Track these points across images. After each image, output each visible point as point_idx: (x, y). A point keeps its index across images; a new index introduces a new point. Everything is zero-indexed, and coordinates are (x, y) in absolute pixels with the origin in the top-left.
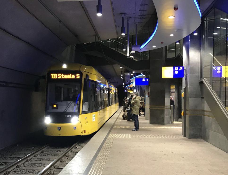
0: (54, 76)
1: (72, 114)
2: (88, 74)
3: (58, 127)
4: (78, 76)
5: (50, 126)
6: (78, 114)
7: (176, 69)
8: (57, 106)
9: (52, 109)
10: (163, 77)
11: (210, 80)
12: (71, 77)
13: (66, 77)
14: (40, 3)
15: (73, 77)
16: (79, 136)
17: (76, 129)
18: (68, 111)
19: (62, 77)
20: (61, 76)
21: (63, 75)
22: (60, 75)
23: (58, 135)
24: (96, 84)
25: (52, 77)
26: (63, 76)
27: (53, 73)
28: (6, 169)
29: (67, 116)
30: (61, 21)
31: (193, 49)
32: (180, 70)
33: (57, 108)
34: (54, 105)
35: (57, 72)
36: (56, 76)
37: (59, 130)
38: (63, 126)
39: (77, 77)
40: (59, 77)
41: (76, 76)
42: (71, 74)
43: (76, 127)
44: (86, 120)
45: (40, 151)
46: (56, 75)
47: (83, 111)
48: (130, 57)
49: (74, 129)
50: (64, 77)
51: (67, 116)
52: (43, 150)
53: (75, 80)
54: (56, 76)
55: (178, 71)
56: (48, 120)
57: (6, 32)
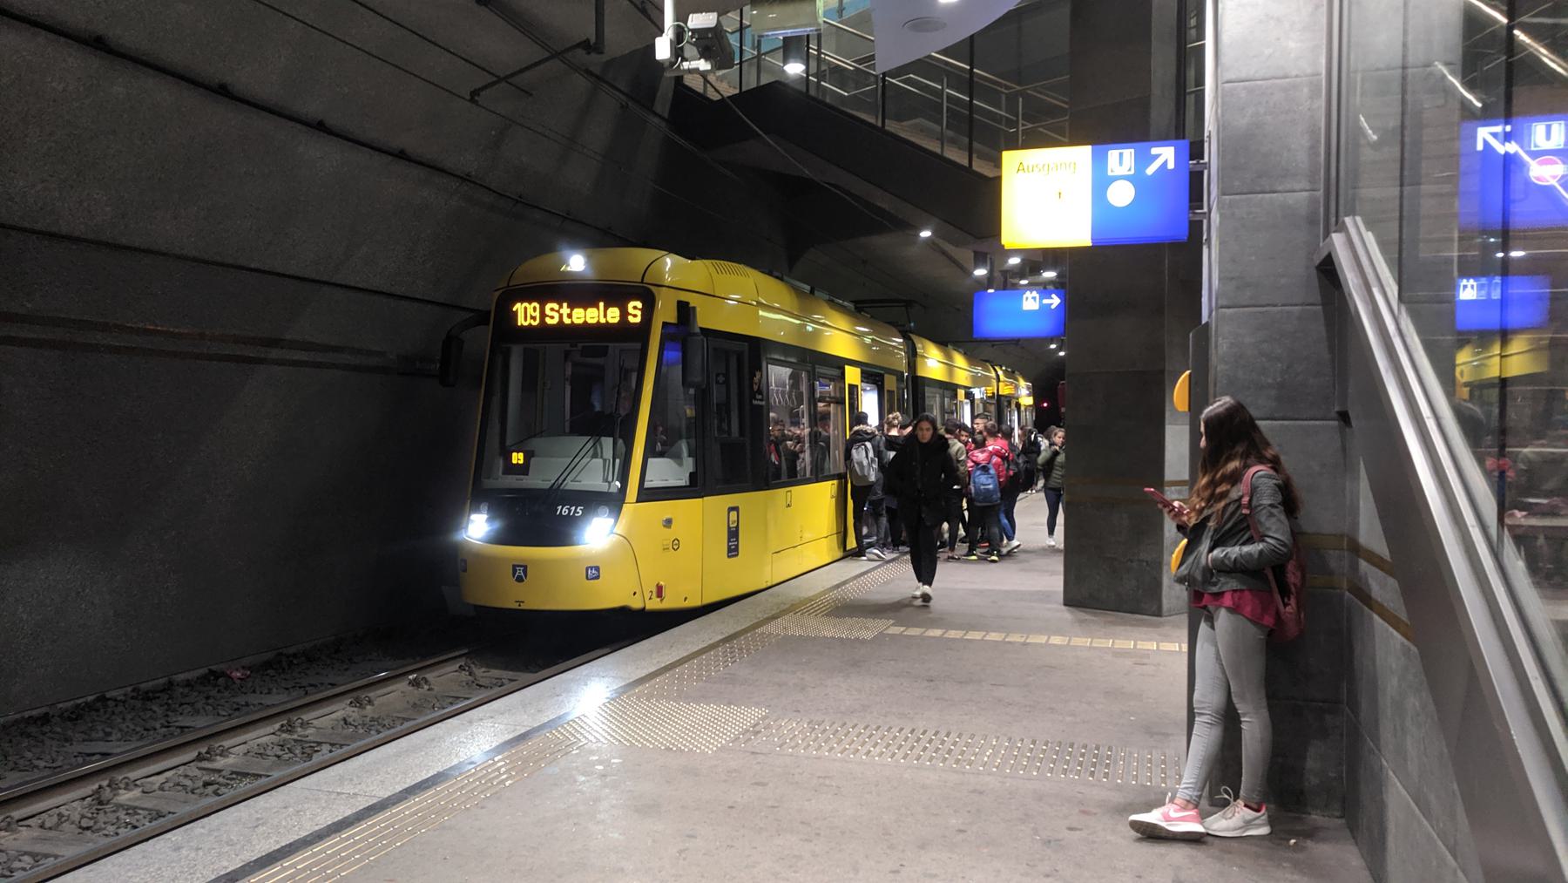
0: (526, 313)
1: (592, 501)
2: (693, 300)
3: (514, 567)
4: (635, 309)
5: (480, 558)
6: (614, 502)
7: (1121, 159)
8: (529, 456)
9: (504, 473)
11: (1000, 393)
12: (605, 316)
13: (580, 316)
15: (613, 315)
16: (624, 611)
17: (598, 577)
18: (570, 485)
19: (561, 316)
20: (557, 313)
21: (565, 310)
22: (552, 309)
23: (515, 606)
25: (521, 321)
26: (568, 311)
27: (522, 301)
29: (565, 511)
32: (1150, 170)
33: (523, 469)
34: (514, 455)
35: (545, 292)
36: (537, 314)
37: (520, 579)
38: (541, 563)
39: (631, 319)
40: (549, 321)
41: (624, 314)
42: (601, 305)
43: (597, 569)
44: (670, 534)
46: (535, 309)
47: (647, 485)
49: (587, 578)
50: (570, 316)
51: (565, 511)
53: (624, 331)
54: (534, 314)
55: (1136, 179)
56: (477, 528)
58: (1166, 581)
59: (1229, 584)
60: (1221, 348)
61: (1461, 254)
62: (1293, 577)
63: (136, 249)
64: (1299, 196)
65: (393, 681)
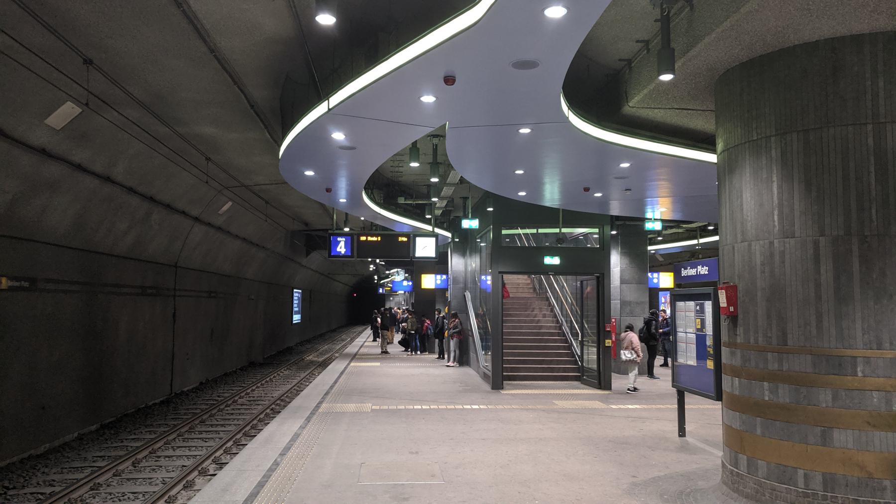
7: (439, 277)
10: (423, 287)
14: (102, 75)
24: (600, 383)
28: (241, 393)
30: (210, 158)
31: (456, 254)
45: (89, 487)
48: (381, 263)
52: (121, 468)
55: (441, 280)
57: (172, 209)
58: (776, 181)
59: (455, 334)
60: (453, 304)
61: (699, 237)
62: (462, 333)
63: (63, 246)
64: (462, 285)
65: (123, 463)
